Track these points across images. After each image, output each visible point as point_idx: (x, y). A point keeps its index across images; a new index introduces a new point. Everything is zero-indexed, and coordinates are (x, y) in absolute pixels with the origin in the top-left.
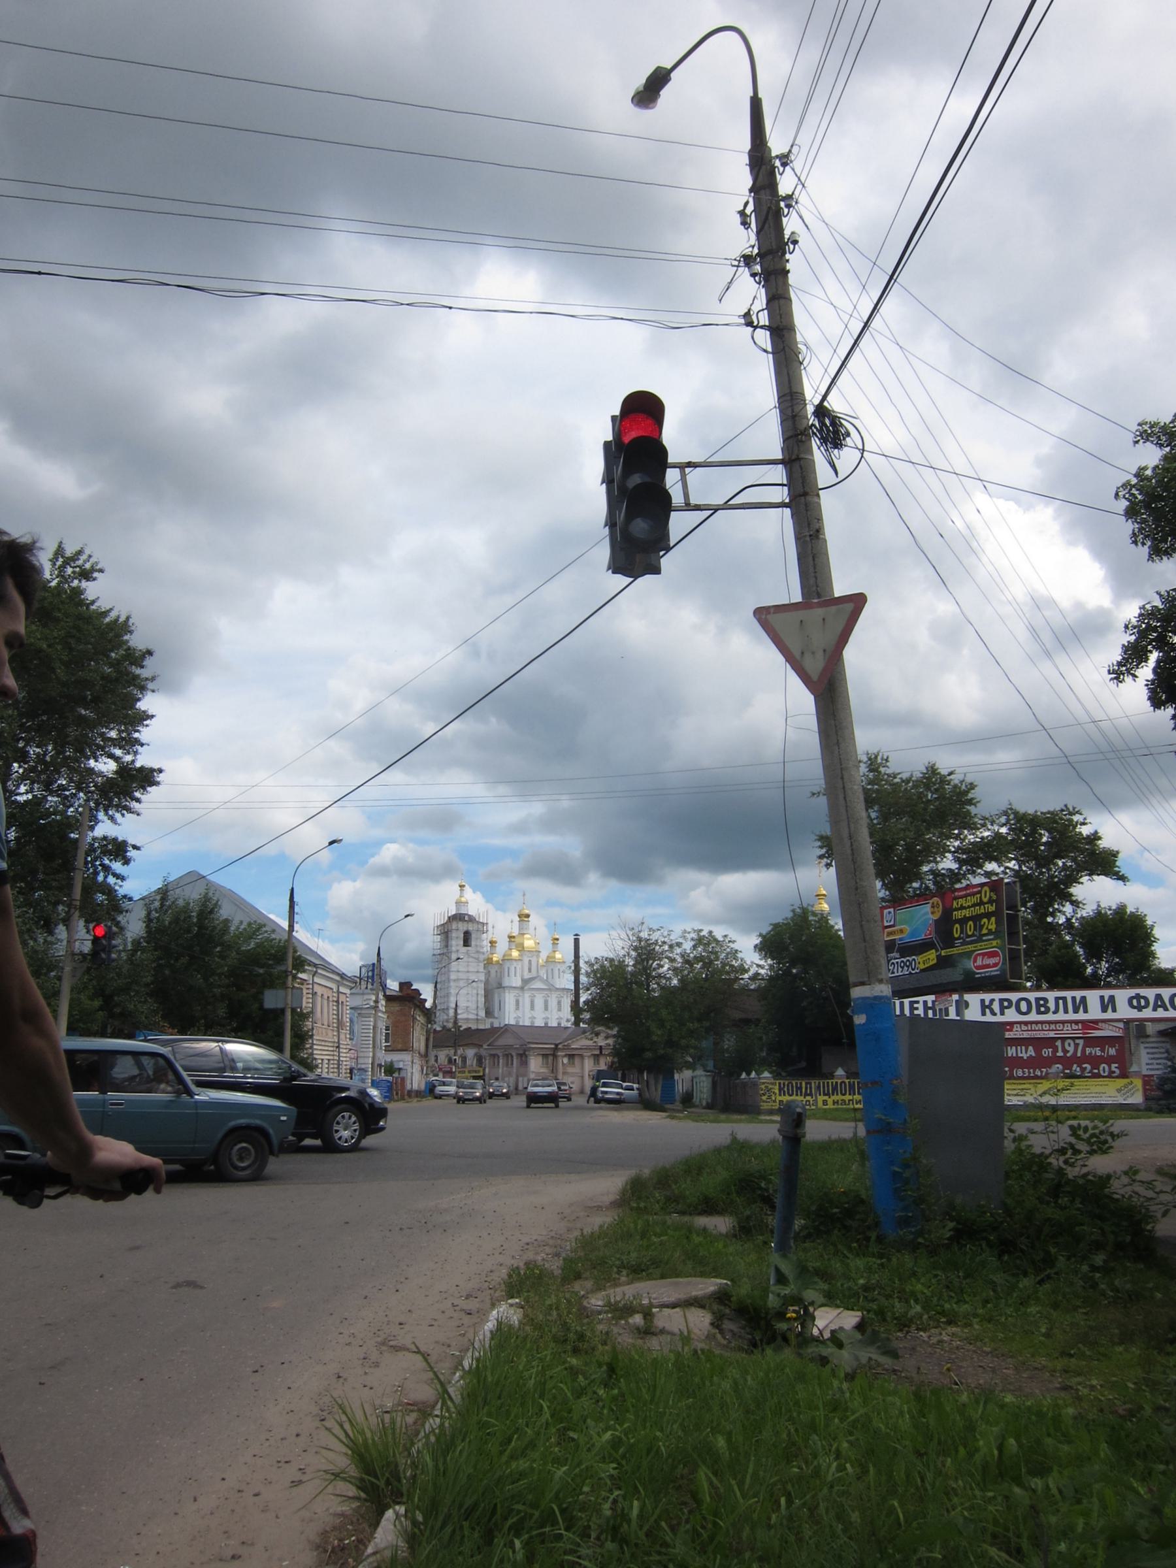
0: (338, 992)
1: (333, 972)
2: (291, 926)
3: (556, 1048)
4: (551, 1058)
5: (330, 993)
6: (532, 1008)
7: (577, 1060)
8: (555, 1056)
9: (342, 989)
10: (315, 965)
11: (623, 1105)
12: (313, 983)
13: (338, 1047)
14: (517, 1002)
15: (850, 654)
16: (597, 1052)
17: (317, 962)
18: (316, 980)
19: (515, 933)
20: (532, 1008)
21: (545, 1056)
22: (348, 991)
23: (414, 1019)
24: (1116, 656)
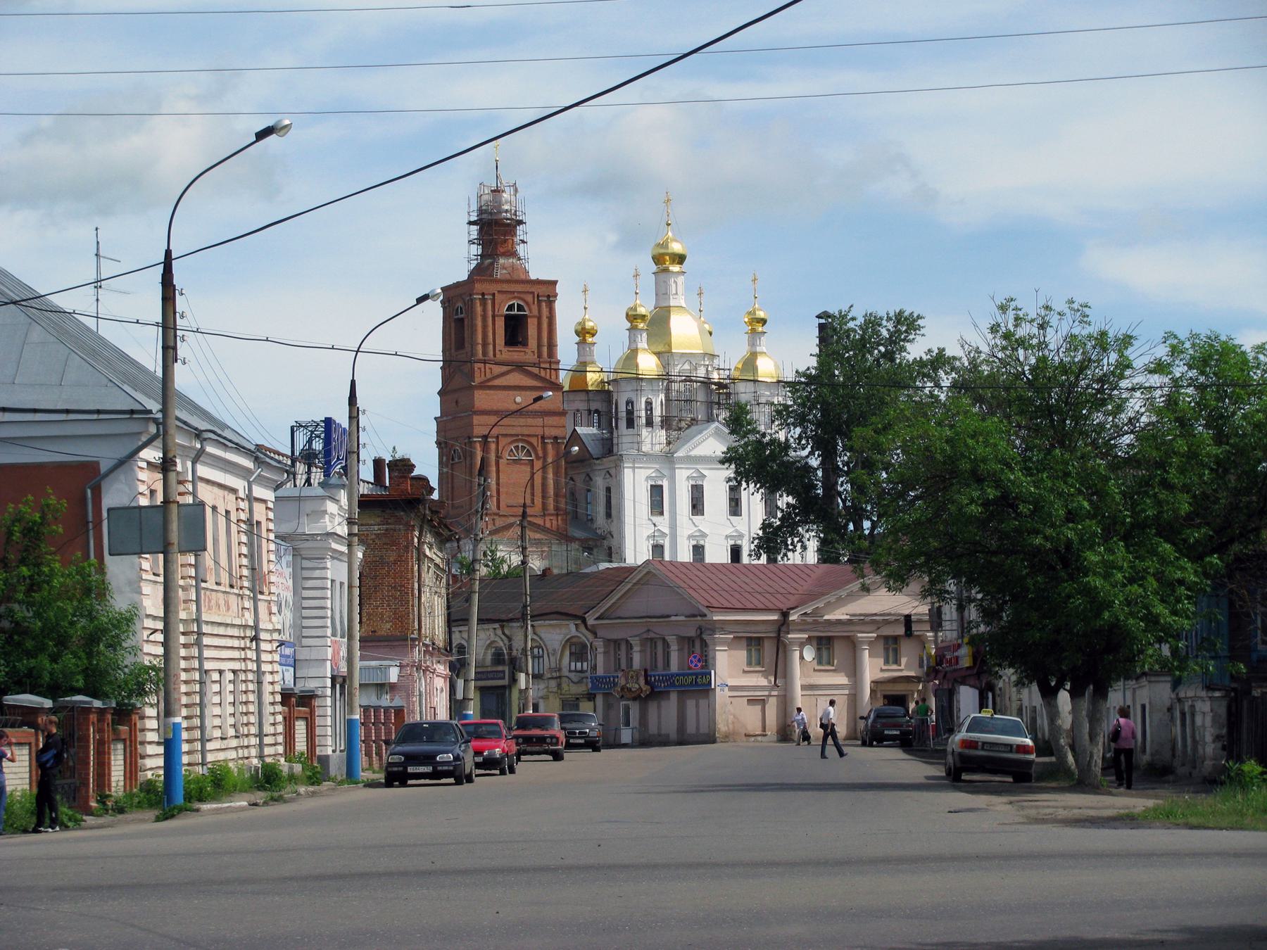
0: (251, 499)
1: (239, 448)
2: (169, 351)
3: (784, 624)
4: (769, 648)
5: (229, 502)
6: (697, 506)
7: (839, 650)
8: (781, 649)
9: (258, 492)
10: (199, 434)
11: (613, 502)
12: (196, 479)
13: (255, 638)
14: (656, 491)
15: (463, 276)
16: (901, 631)
17: (202, 425)
18: (202, 471)
19: (646, 308)
20: (697, 506)
21: (754, 643)
22: (269, 495)
23: (421, 556)
24: (538, 255)
